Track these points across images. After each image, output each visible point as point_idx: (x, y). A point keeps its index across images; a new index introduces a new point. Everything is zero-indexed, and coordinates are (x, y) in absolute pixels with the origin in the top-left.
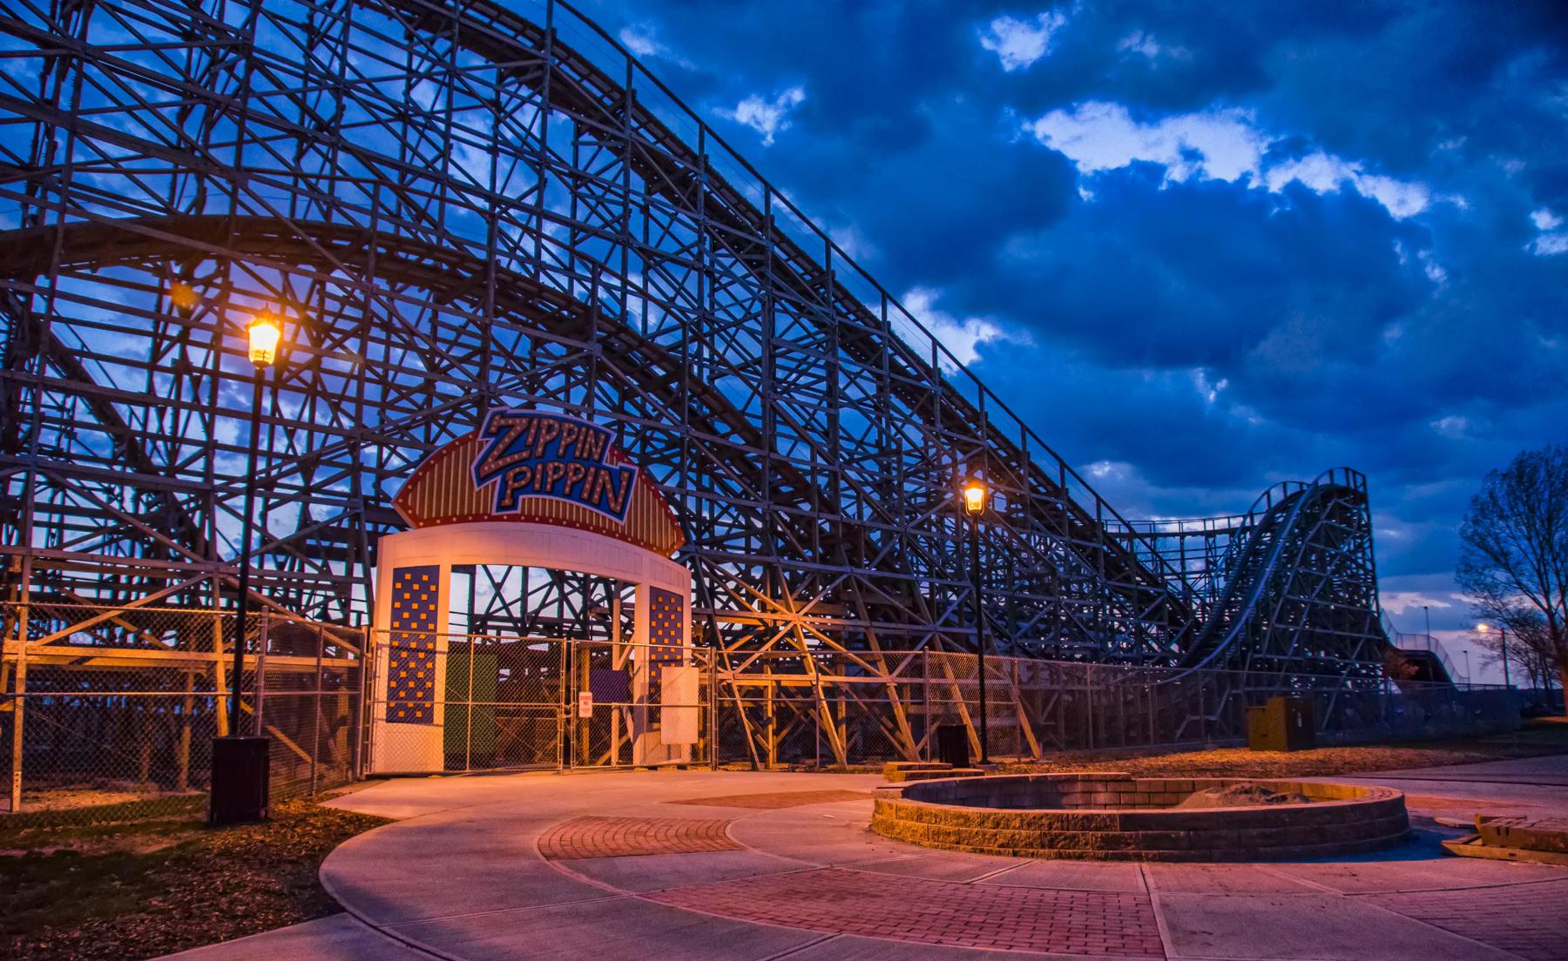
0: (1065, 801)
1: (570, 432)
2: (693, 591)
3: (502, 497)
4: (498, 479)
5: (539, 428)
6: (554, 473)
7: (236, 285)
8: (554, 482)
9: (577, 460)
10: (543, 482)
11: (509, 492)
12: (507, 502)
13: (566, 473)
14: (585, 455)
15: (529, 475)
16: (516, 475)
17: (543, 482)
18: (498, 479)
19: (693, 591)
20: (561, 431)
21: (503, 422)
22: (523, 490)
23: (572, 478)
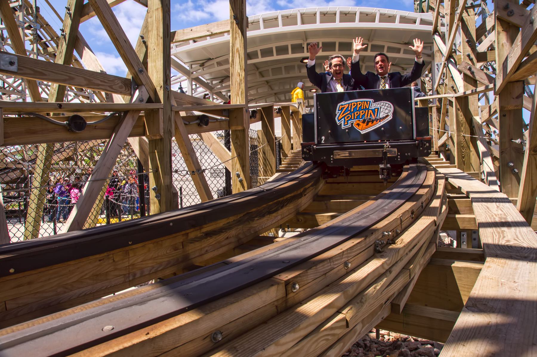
0: (102, 119)
1: (360, 104)
2: (114, 294)
3: (344, 123)
4: (343, 119)
5: (351, 105)
6: (354, 106)
7: (421, 183)
8: (357, 116)
9: (362, 110)
10: (354, 117)
11: (346, 121)
12: (346, 123)
13: (360, 113)
14: (364, 108)
15: (350, 116)
16: (347, 117)
17: (354, 117)
18: (343, 119)
19: (114, 294)
20: (357, 104)
21: (342, 107)
22: (349, 120)
23: (361, 114)
